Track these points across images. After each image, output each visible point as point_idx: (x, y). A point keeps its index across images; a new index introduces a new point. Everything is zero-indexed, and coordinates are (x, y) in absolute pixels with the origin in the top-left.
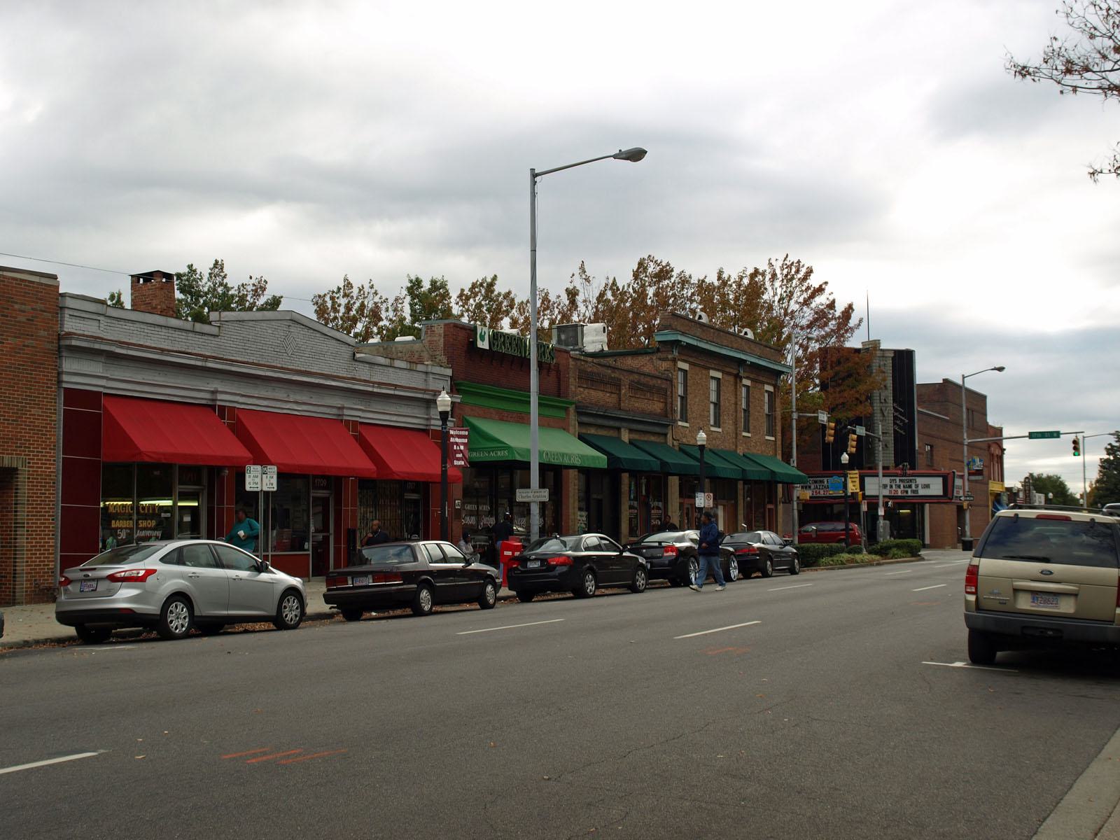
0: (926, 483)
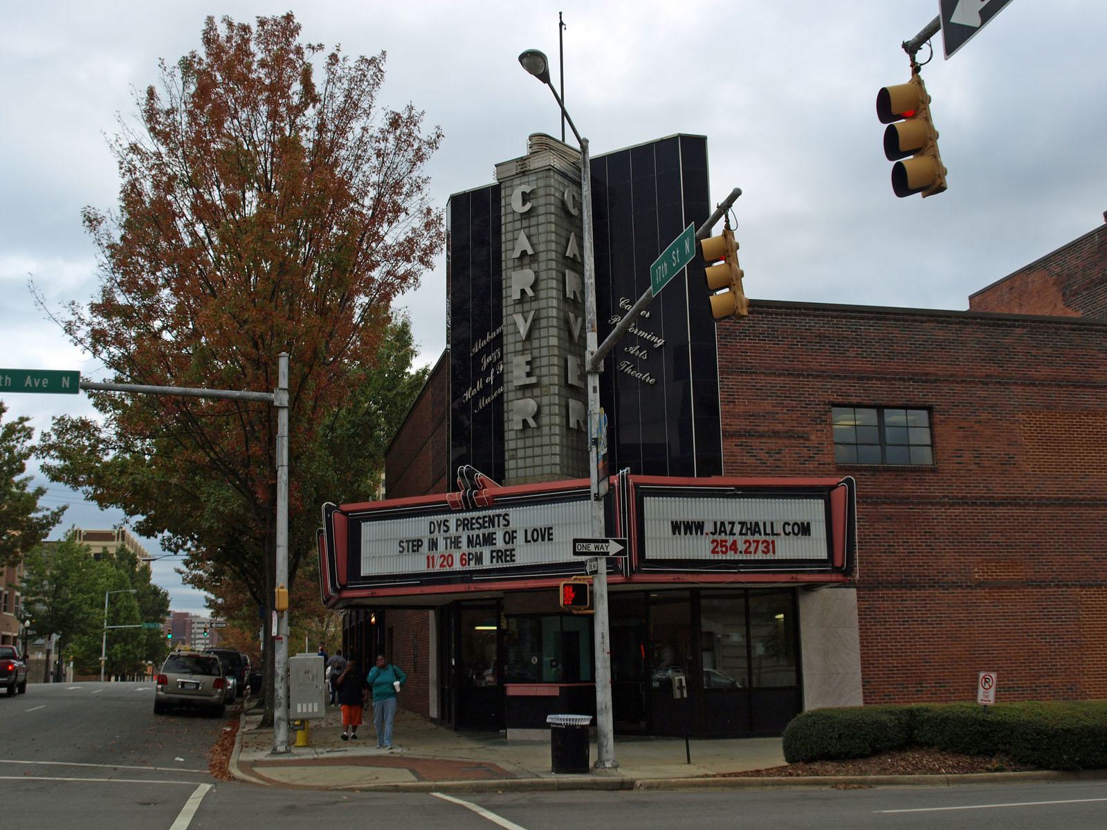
0: (541, 523)
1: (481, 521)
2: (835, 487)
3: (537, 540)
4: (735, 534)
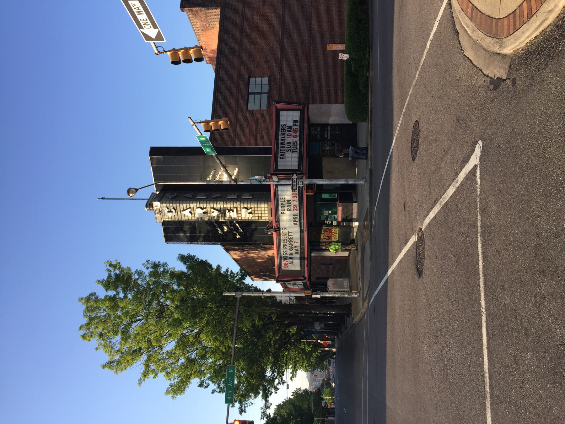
2: (276, 107)
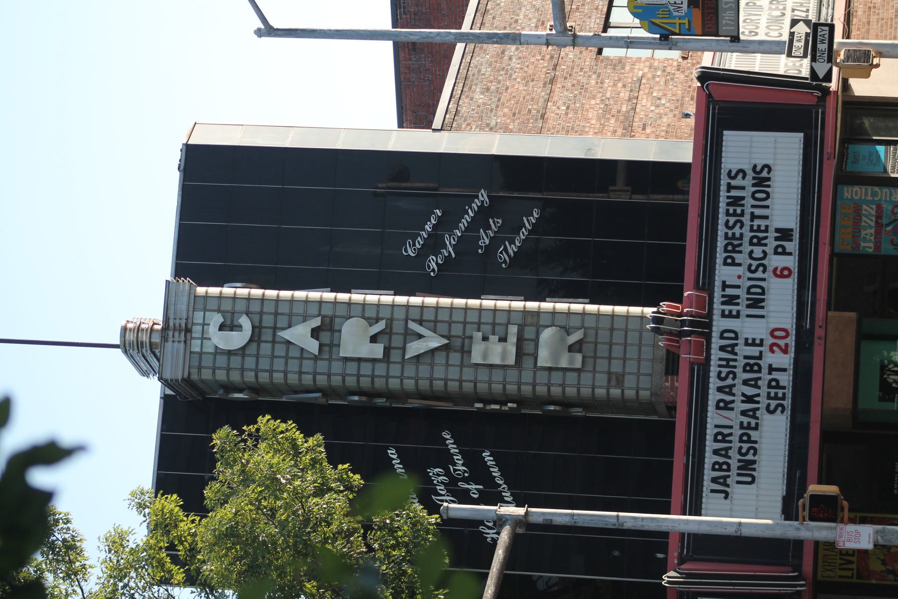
1: (732, 220)
3: (762, 288)
4: (761, 352)
